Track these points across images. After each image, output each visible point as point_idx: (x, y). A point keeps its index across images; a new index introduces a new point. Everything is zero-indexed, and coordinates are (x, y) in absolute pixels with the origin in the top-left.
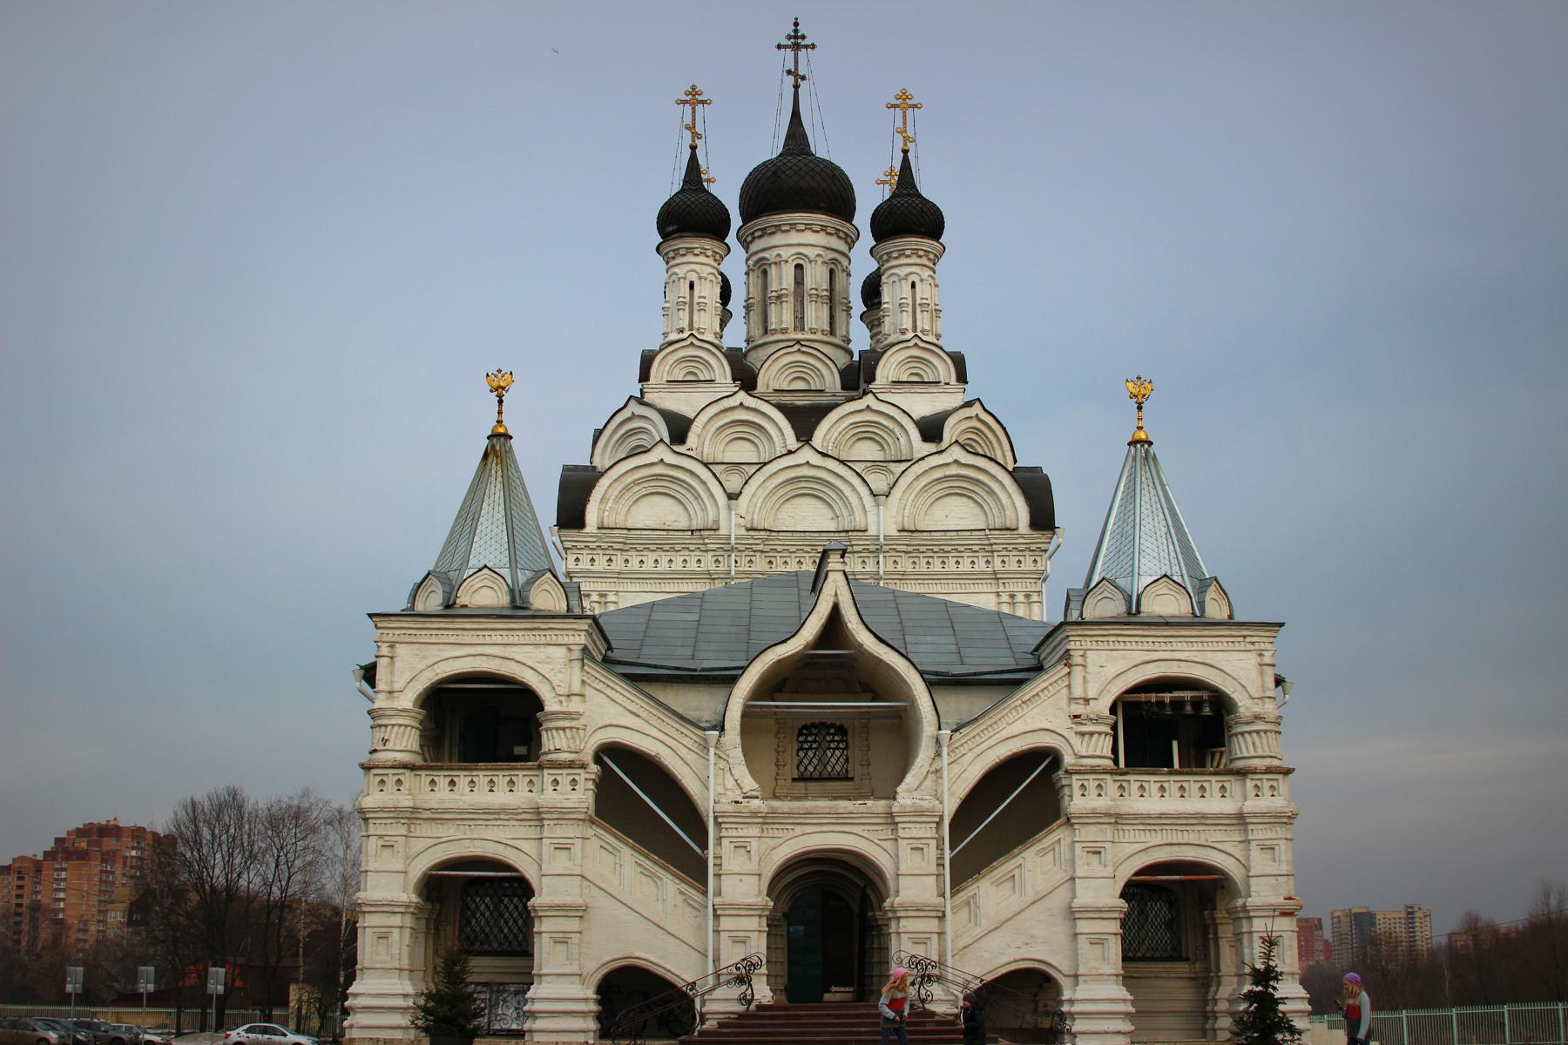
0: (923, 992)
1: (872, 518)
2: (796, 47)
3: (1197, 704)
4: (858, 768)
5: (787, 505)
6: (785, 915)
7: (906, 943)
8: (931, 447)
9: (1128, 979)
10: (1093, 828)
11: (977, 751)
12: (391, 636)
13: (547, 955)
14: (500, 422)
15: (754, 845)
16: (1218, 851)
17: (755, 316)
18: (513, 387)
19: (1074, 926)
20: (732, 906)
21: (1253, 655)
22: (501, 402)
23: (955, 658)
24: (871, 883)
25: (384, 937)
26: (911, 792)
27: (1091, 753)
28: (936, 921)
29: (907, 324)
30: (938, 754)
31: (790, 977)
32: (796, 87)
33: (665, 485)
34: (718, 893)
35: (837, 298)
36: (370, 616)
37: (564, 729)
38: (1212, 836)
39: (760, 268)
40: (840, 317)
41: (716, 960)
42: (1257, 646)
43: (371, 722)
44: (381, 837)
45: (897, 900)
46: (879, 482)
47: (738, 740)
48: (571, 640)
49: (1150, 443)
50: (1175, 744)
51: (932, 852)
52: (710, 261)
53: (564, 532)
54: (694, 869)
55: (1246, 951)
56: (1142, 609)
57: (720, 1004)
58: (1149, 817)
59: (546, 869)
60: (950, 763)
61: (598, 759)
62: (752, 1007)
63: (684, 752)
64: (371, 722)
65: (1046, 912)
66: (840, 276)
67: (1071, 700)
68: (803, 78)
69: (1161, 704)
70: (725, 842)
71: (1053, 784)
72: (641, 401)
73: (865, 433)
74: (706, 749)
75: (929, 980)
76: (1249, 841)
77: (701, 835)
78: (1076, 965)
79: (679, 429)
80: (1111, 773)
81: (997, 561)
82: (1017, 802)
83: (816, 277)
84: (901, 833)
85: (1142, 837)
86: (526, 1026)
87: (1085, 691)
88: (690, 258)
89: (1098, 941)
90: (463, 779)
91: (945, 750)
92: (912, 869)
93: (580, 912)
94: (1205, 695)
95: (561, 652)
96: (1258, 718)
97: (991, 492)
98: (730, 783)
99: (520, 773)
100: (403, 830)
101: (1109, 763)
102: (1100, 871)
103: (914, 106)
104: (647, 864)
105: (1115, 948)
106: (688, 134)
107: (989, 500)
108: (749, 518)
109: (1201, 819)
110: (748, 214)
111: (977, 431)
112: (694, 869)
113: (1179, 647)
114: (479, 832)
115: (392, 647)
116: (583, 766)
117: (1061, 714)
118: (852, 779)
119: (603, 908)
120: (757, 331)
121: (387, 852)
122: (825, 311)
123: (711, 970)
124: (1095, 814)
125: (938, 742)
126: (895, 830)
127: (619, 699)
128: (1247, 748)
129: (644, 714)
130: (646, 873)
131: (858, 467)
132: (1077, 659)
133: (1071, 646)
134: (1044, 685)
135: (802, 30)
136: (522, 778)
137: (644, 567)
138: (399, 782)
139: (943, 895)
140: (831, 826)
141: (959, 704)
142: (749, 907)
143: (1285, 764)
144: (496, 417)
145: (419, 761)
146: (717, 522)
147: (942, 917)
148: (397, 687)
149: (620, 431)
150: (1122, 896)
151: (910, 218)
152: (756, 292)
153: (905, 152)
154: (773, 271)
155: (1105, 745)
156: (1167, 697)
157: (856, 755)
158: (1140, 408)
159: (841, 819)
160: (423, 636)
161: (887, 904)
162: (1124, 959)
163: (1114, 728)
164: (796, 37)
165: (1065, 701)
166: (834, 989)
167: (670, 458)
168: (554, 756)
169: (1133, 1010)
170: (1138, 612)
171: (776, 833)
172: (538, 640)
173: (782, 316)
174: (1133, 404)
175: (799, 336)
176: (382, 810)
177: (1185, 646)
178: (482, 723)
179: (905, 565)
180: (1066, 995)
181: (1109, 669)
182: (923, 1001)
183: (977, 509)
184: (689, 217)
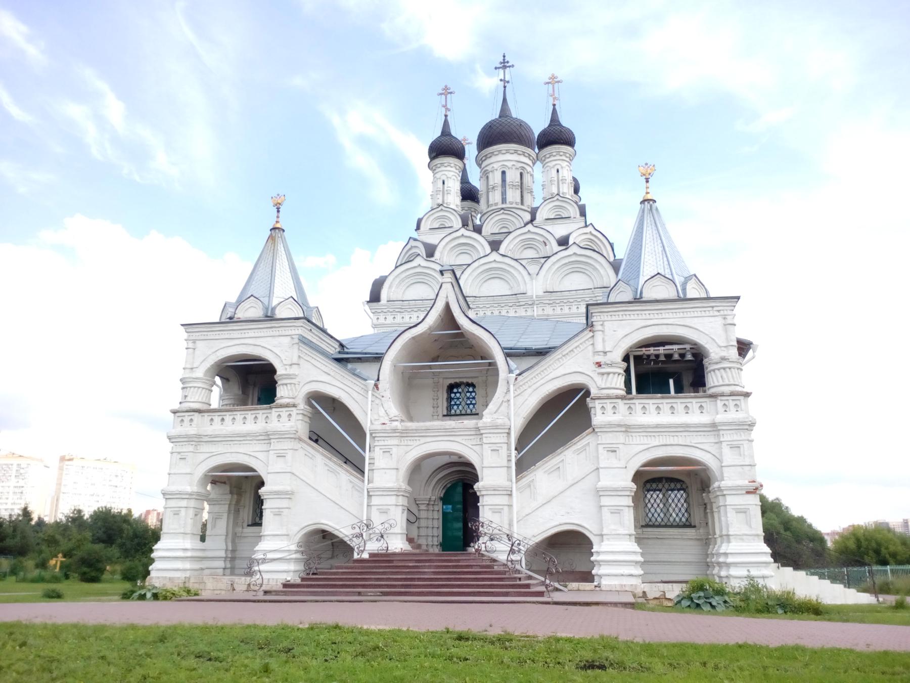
5: (485, 284)
9: (639, 540)
10: (610, 435)
11: (534, 387)
12: (195, 336)
14: (277, 222)
15: (394, 450)
16: (699, 450)
19: (600, 501)
20: (378, 489)
22: (278, 211)
25: (176, 514)
26: (489, 415)
27: (608, 385)
28: (506, 497)
30: (508, 390)
32: (505, 87)
35: (525, 186)
37: (286, 384)
42: (722, 313)
43: (182, 386)
44: (179, 453)
46: (533, 269)
48: (293, 332)
49: (655, 201)
50: (671, 382)
51: (504, 451)
52: (453, 169)
54: (355, 464)
55: (723, 518)
56: (644, 295)
58: (649, 426)
60: (515, 399)
63: (355, 395)
64: (182, 386)
65: (578, 492)
69: (657, 356)
70: (377, 449)
73: (528, 245)
78: (602, 529)
79: (430, 251)
80: (622, 398)
83: (513, 176)
84: (485, 440)
85: (645, 440)
87: (604, 346)
88: (443, 168)
89: (616, 511)
93: (288, 495)
94: (688, 347)
96: (723, 359)
97: (595, 269)
98: (382, 412)
100: (191, 448)
102: (614, 462)
103: (558, 82)
104: (331, 464)
105: (629, 517)
106: (444, 109)
107: (594, 273)
109: (686, 428)
111: (591, 241)
112: (355, 464)
113: (667, 315)
114: (235, 448)
115: (194, 342)
116: (294, 406)
117: (593, 364)
119: (308, 494)
121: (182, 461)
122: (519, 192)
124: (610, 425)
127: (319, 365)
128: (713, 379)
129: (332, 374)
131: (523, 262)
132: (597, 327)
134: (576, 344)
135: (507, 59)
138: (191, 420)
140: (452, 438)
142: (624, 489)
143: (746, 390)
144: (275, 219)
147: (510, 495)
153: (554, 105)
154: (490, 175)
155: (620, 381)
156: (661, 350)
158: (647, 182)
160: (211, 335)
161: (716, 484)
163: (627, 371)
165: (591, 354)
167: (424, 263)
169: (642, 559)
171: (409, 443)
174: (643, 179)
175: (504, 206)
177: (671, 315)
178: (253, 381)
179: (549, 310)
181: (622, 333)
184: (445, 148)
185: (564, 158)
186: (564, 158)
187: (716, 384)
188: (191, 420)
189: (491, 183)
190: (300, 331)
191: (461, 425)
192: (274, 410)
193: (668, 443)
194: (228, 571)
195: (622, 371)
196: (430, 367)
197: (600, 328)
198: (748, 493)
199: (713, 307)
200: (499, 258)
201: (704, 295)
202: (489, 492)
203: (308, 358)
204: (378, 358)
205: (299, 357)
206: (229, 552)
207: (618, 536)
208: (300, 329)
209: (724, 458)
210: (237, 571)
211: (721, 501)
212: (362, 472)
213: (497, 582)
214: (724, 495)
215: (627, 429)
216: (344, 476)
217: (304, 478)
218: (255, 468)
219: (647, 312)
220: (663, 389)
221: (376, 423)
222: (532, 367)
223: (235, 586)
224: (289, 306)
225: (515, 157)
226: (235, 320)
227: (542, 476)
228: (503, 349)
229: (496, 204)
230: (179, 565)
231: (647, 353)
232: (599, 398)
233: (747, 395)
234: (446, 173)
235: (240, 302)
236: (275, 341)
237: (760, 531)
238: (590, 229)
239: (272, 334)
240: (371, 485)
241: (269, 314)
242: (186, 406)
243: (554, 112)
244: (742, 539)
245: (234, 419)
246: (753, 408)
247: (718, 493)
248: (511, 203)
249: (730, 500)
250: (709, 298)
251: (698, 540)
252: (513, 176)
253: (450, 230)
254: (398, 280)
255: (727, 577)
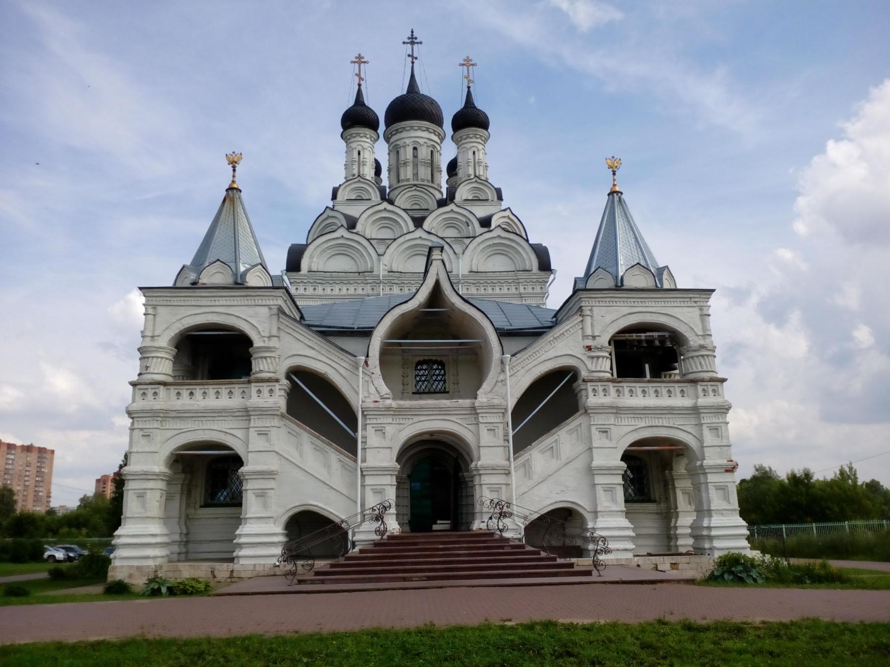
0: (501, 524)
1: (454, 265)
2: (413, 43)
3: (662, 340)
4: (451, 385)
5: (331, 260)
6: (409, 476)
7: (485, 492)
8: (485, 230)
9: (628, 514)
10: (602, 416)
11: (527, 368)
12: (155, 301)
13: (251, 505)
14: (233, 182)
15: (389, 430)
16: (681, 431)
17: (394, 174)
18: (242, 162)
19: (594, 480)
21: (697, 309)
22: (234, 170)
23: (508, 324)
24: (460, 455)
27: (598, 369)
29: (471, 171)
31: (412, 514)
32: (413, 63)
33: (343, 250)
34: (364, 461)
36: (141, 288)
37: (265, 358)
38: (678, 422)
39: (395, 151)
40: (436, 174)
41: (363, 505)
42: (699, 304)
44: (142, 429)
45: (480, 463)
46: (458, 248)
47: (378, 362)
48: (271, 302)
50: (647, 366)
51: (500, 432)
52: (369, 140)
53: (289, 274)
54: (348, 445)
55: (704, 495)
56: (625, 283)
57: (363, 534)
59: (251, 448)
60: (510, 378)
61: (288, 377)
62: (385, 537)
63: (342, 371)
66: (436, 155)
67: (585, 337)
68: (416, 58)
69: (640, 341)
70: (369, 427)
71: (574, 390)
72: (332, 209)
74: (357, 369)
75: (505, 516)
76: (702, 424)
77: (352, 419)
79: (352, 224)
81: (522, 288)
82: (552, 401)
83: (424, 153)
84: (481, 420)
86: (235, 554)
89: (609, 489)
90: (198, 392)
91: (507, 367)
92: (489, 445)
93: (269, 475)
94: (667, 334)
95: (264, 311)
97: (518, 252)
98: (372, 390)
99: (237, 386)
101: (609, 375)
102: (608, 443)
103: (473, 65)
104: (319, 443)
106: (357, 79)
107: (517, 256)
108: (389, 266)
109: (670, 411)
110: (388, 123)
112: (348, 445)
113: (650, 304)
116: (277, 381)
118: (448, 392)
119: (289, 474)
120: (394, 182)
122: (430, 169)
123: (359, 511)
125: (502, 362)
126: (477, 418)
128: (692, 366)
129: (317, 348)
130: (317, 449)
131: (448, 240)
133: (583, 304)
134: (567, 328)
135: (415, 35)
136: (237, 389)
137: (333, 293)
139: (509, 460)
140: (437, 417)
141: (512, 344)
142: (385, 469)
143: (720, 375)
145: (170, 380)
146: (372, 268)
147: (508, 474)
148: (157, 333)
149: (323, 225)
150: (622, 460)
151: (470, 119)
152: (394, 162)
153: (469, 87)
154: (402, 151)
156: (643, 336)
157: (450, 378)
158: (614, 174)
159: (444, 412)
161: (473, 465)
162: (626, 501)
164: (412, 38)
166: (439, 522)
167: (347, 235)
168: (259, 375)
170: (622, 285)
171: (401, 421)
172: (250, 303)
173: (407, 173)
174: (610, 171)
175: (416, 183)
176: (143, 411)
177: (653, 304)
178: (214, 355)
180: (590, 525)
181: (609, 318)
182: (501, 531)
183: (510, 261)
184: (357, 118)
185: (479, 140)
186: (479, 140)
187: (695, 370)
188: (155, 394)
189: (402, 158)
190: (280, 302)
191: (455, 405)
192: (253, 384)
193: (654, 424)
194: (183, 557)
195: (607, 355)
196: (400, 344)
197: (589, 313)
198: (727, 471)
199: (690, 298)
200: (425, 236)
201: (673, 287)
202: (488, 472)
203: (290, 331)
204: (366, 333)
205: (279, 328)
206: (183, 536)
207: (611, 513)
208: (279, 300)
209: (705, 439)
210: (191, 556)
211: (477, 480)
212: (355, 453)
213: (493, 559)
214: (480, 475)
215: (617, 411)
216: (335, 457)
217: (289, 458)
218: (233, 446)
219: (632, 300)
220: (638, 374)
221: (368, 400)
222: (525, 348)
223: (216, 573)
224: (259, 274)
225: (425, 134)
226: (199, 285)
227: (537, 456)
228: (496, 329)
229: (408, 180)
230: (150, 552)
231: (630, 338)
232: (591, 381)
233: (723, 380)
234: (362, 143)
235: (588, 275)
236: (251, 311)
237: (736, 506)
238: (508, 213)
239: (246, 303)
240: (364, 465)
241: (239, 281)
242: (148, 378)
243: (469, 95)
244: (722, 514)
245: (205, 393)
246: (728, 393)
247: (475, 473)
248: (423, 180)
249: (486, 479)
250: (676, 290)
251: (657, 513)
252: (424, 153)
253: (370, 204)
254: (319, 250)
255: (710, 549)
